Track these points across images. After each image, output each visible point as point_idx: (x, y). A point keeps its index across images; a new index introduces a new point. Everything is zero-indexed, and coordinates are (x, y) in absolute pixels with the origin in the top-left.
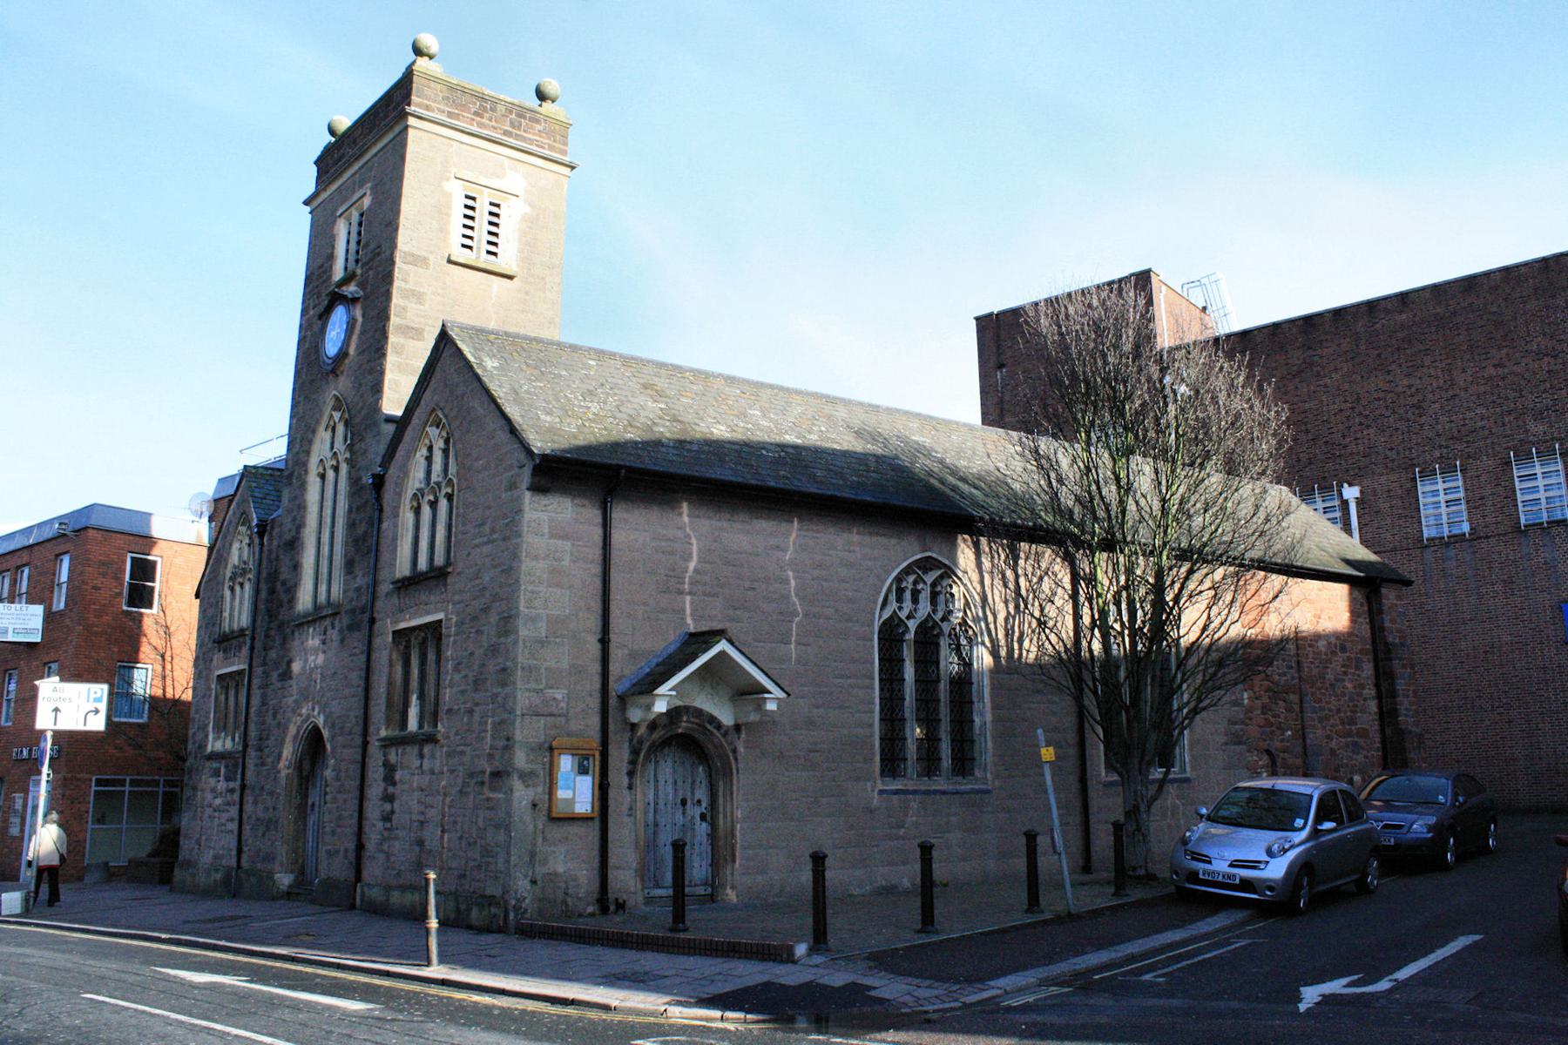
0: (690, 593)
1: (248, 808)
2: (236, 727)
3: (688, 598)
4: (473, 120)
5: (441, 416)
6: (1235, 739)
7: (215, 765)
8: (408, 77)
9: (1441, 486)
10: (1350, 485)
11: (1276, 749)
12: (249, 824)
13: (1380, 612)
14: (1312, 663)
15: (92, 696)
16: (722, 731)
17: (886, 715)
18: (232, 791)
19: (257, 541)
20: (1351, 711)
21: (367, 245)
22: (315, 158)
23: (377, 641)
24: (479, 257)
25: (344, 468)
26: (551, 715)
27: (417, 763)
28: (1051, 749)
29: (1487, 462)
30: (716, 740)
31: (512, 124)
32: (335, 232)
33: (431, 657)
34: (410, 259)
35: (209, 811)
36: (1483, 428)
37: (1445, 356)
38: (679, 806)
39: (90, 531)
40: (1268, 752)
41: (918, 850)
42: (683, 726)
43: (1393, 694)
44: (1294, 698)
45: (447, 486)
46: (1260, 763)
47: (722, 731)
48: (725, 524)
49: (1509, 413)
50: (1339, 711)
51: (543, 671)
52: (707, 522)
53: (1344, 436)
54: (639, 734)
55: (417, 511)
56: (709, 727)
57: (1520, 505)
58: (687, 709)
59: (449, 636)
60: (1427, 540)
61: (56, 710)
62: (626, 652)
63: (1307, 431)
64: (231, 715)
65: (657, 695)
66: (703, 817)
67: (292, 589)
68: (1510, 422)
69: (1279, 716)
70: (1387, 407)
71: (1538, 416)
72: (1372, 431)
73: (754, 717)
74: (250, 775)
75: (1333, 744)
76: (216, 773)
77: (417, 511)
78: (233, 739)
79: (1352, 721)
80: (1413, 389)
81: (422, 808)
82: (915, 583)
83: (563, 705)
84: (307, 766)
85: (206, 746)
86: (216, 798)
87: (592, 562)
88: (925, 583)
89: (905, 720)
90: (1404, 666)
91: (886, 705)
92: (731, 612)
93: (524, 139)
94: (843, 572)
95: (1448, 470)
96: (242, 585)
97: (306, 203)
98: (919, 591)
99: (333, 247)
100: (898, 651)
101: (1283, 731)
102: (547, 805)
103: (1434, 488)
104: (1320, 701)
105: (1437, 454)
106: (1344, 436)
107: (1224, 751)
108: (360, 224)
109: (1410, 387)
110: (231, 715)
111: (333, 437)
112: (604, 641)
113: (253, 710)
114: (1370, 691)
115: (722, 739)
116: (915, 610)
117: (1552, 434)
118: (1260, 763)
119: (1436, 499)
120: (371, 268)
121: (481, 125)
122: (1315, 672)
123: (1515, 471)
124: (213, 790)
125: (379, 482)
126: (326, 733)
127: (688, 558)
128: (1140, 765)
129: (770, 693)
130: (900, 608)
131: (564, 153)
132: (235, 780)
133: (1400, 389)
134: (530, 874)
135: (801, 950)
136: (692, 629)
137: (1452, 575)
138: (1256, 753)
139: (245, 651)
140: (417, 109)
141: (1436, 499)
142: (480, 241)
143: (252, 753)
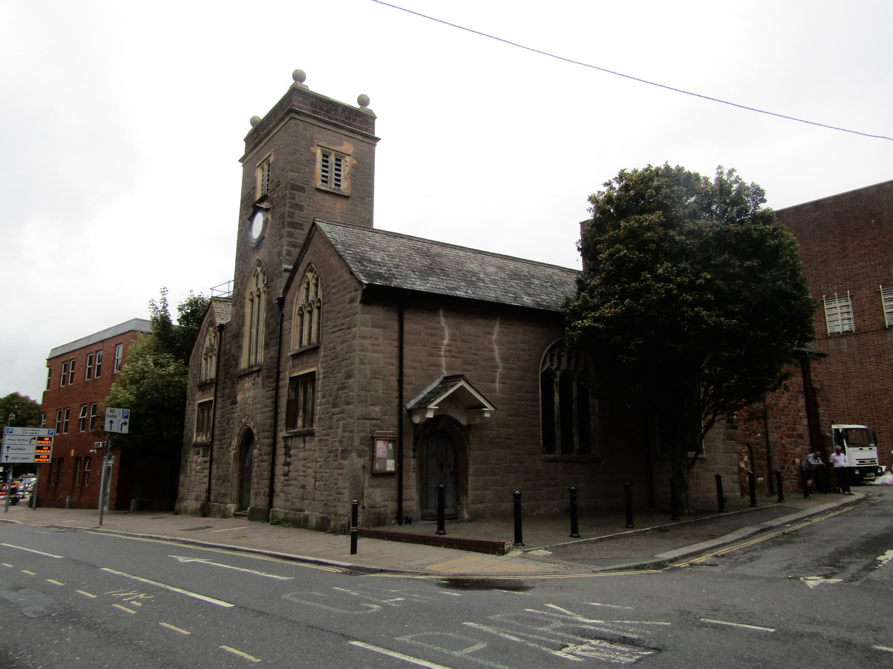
0: (445, 356)
1: (214, 470)
5: (314, 267)
7: (197, 449)
9: (838, 305)
12: (214, 479)
13: (809, 371)
18: (205, 462)
19: (218, 334)
21: (273, 181)
23: (281, 383)
24: (331, 187)
25: (263, 296)
26: (373, 419)
27: (302, 445)
32: (256, 175)
33: (310, 390)
35: (193, 473)
36: (864, 273)
40: (748, 445)
43: (817, 415)
45: (317, 302)
49: (879, 264)
50: (786, 424)
55: (302, 316)
56: (454, 426)
59: (318, 379)
60: (830, 334)
61: (111, 422)
64: (206, 423)
66: (451, 473)
67: (237, 359)
69: (753, 426)
73: (478, 421)
74: (215, 453)
75: (784, 442)
76: (198, 453)
77: (302, 316)
78: (206, 435)
79: (794, 430)
85: (192, 439)
86: (197, 466)
87: (394, 340)
90: (823, 400)
92: (465, 366)
93: (352, 125)
95: (842, 296)
96: (211, 357)
97: (241, 161)
99: (255, 183)
101: (756, 434)
105: (836, 287)
107: (724, 443)
108: (269, 171)
110: (206, 423)
111: (257, 280)
112: (400, 381)
113: (217, 421)
114: (803, 413)
116: (560, 366)
120: (275, 193)
121: (329, 118)
122: (773, 402)
123: (882, 296)
124: (196, 462)
125: (281, 302)
126: (255, 431)
127: (442, 338)
129: (487, 408)
130: (552, 365)
132: (208, 456)
138: (741, 445)
139: (213, 390)
142: (331, 178)
143: (216, 443)
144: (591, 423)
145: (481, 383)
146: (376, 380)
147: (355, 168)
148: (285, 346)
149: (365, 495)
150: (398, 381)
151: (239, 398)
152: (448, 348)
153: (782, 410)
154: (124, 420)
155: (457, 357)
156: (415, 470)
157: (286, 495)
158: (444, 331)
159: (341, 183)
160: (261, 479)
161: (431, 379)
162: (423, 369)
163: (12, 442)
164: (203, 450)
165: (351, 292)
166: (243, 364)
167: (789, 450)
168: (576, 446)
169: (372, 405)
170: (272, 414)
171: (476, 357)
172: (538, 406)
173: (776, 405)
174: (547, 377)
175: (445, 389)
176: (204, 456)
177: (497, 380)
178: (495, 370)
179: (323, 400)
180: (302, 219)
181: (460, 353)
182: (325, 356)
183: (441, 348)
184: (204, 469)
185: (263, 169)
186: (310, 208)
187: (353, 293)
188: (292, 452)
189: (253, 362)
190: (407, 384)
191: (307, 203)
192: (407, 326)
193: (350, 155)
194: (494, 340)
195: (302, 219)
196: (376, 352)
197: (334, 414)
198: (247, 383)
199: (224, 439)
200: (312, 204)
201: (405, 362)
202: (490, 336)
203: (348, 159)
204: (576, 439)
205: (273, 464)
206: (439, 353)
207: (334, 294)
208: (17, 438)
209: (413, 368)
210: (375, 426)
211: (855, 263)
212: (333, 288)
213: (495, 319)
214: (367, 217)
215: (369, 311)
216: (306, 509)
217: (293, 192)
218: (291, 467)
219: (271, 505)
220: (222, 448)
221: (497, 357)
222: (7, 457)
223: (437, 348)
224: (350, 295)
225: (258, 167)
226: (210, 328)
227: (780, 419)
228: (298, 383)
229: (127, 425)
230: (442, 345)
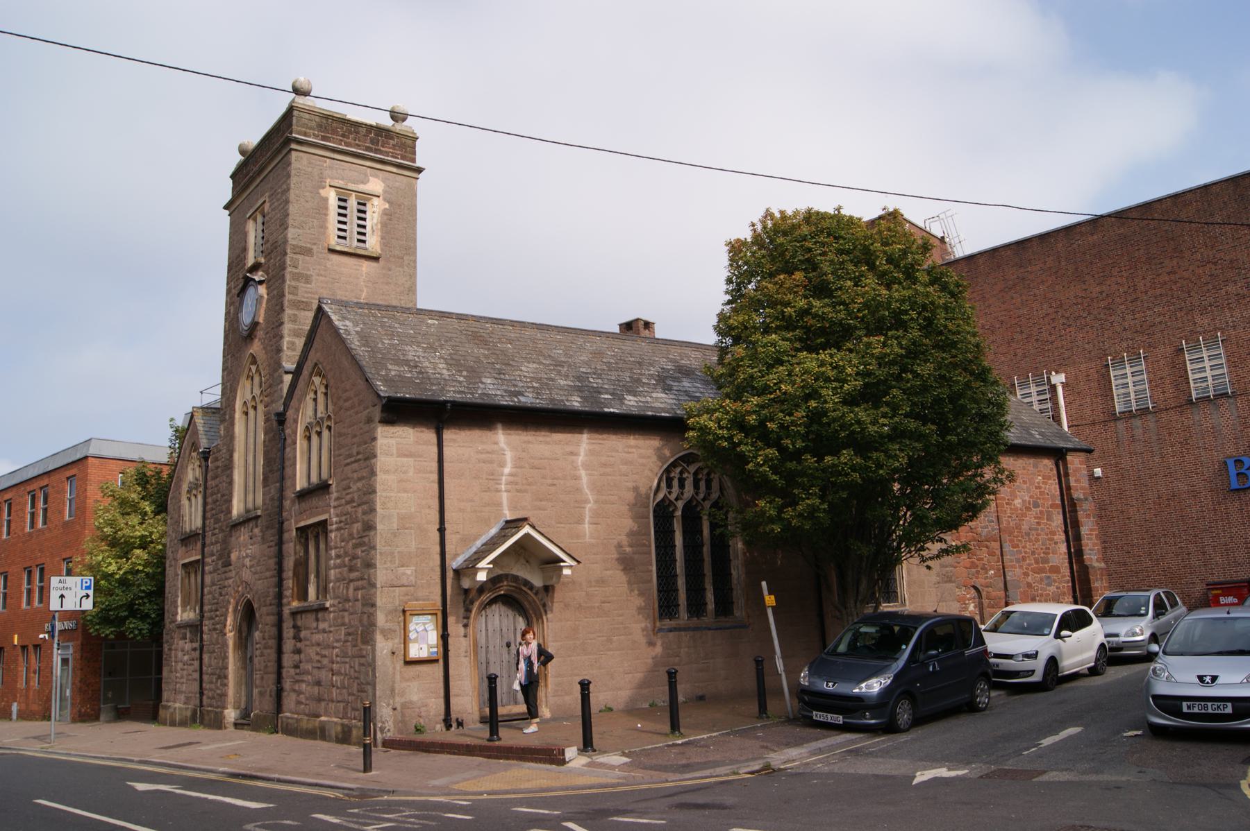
0: (506, 491)
2: (196, 602)
4: (341, 140)
6: (946, 579)
7: (183, 631)
8: (291, 110)
10: (1057, 372)
11: (981, 585)
14: (1009, 517)
15: (84, 585)
17: (662, 573)
18: (194, 649)
20: (1044, 553)
22: (230, 173)
23: (286, 536)
24: (352, 244)
26: (403, 586)
28: (773, 597)
29: (1165, 350)
30: (530, 599)
31: (372, 142)
32: (246, 230)
33: (322, 546)
34: (297, 250)
36: (1160, 323)
37: (1128, 267)
39: (89, 459)
41: (666, 675)
44: (996, 545)
46: (968, 596)
49: (1181, 309)
50: (1033, 553)
51: (396, 554)
52: (517, 437)
53: (1051, 334)
54: (470, 597)
55: (309, 439)
56: (524, 588)
57: (1191, 382)
58: (506, 576)
61: (62, 596)
62: (458, 536)
63: (1022, 332)
65: (479, 568)
68: (1182, 317)
69: (982, 559)
70: (1084, 310)
71: (1204, 311)
72: (1072, 329)
74: (205, 636)
76: (184, 638)
77: (309, 439)
78: (195, 611)
79: (1046, 561)
80: (1104, 295)
81: (318, 658)
82: (681, 473)
83: (412, 578)
84: (245, 628)
88: (689, 473)
89: (677, 576)
91: (662, 565)
92: (538, 503)
93: (381, 152)
94: (624, 468)
96: (195, 496)
97: (226, 208)
98: (685, 479)
100: (670, 525)
101: (986, 571)
102: (403, 652)
103: (1122, 372)
104: (1017, 546)
105: (1125, 344)
106: (1051, 334)
109: (1101, 293)
112: (442, 530)
115: (535, 598)
116: (682, 494)
117: (1215, 325)
118: (968, 596)
119: (1124, 381)
121: (347, 144)
122: (1012, 524)
123: (1186, 356)
124: (183, 651)
125: (281, 419)
127: (502, 465)
128: (856, 603)
129: (564, 561)
130: (670, 493)
131: (414, 160)
133: (1094, 295)
134: (391, 701)
135: (571, 752)
136: (508, 519)
137: (1140, 440)
139: (199, 545)
140: (297, 136)
141: (1124, 381)
142: (352, 232)
143: (206, 622)
144: (733, 571)
147: (386, 214)
148: (288, 483)
149: (396, 691)
150: (445, 529)
151: (234, 556)
152: (511, 479)
153: (1028, 534)
154: (84, 593)
155: (525, 491)
157: (298, 696)
158: (504, 454)
159: (367, 238)
160: (266, 673)
161: (487, 523)
162: (475, 511)
164: (191, 632)
165: (367, 408)
166: (237, 508)
167: (1037, 590)
168: (711, 606)
169: (402, 566)
170: (275, 580)
171: (553, 489)
172: (650, 553)
173: (1018, 527)
174: (663, 513)
175: (506, 537)
176: (191, 641)
177: (587, 520)
178: (583, 505)
179: (338, 561)
180: (310, 295)
181: (529, 485)
182: (337, 499)
183: (501, 480)
184: (193, 660)
185: (255, 220)
187: (371, 409)
188: (303, 634)
189: (250, 505)
190: (452, 534)
191: (315, 271)
193: (379, 197)
194: (580, 464)
195: (310, 295)
196: (405, 491)
197: (352, 581)
198: (243, 535)
199: (217, 616)
200: (323, 273)
202: (573, 457)
203: (376, 201)
204: (710, 596)
205: (280, 652)
206: (497, 486)
207: (347, 410)
209: (460, 510)
211: (1149, 308)
212: (346, 401)
216: (322, 713)
217: (295, 256)
218: (302, 656)
219: (279, 707)
220: (215, 629)
221: (585, 487)
223: (493, 480)
224: (367, 411)
225: (249, 218)
226: (193, 454)
227: (1024, 547)
228: (307, 535)
230: (502, 475)
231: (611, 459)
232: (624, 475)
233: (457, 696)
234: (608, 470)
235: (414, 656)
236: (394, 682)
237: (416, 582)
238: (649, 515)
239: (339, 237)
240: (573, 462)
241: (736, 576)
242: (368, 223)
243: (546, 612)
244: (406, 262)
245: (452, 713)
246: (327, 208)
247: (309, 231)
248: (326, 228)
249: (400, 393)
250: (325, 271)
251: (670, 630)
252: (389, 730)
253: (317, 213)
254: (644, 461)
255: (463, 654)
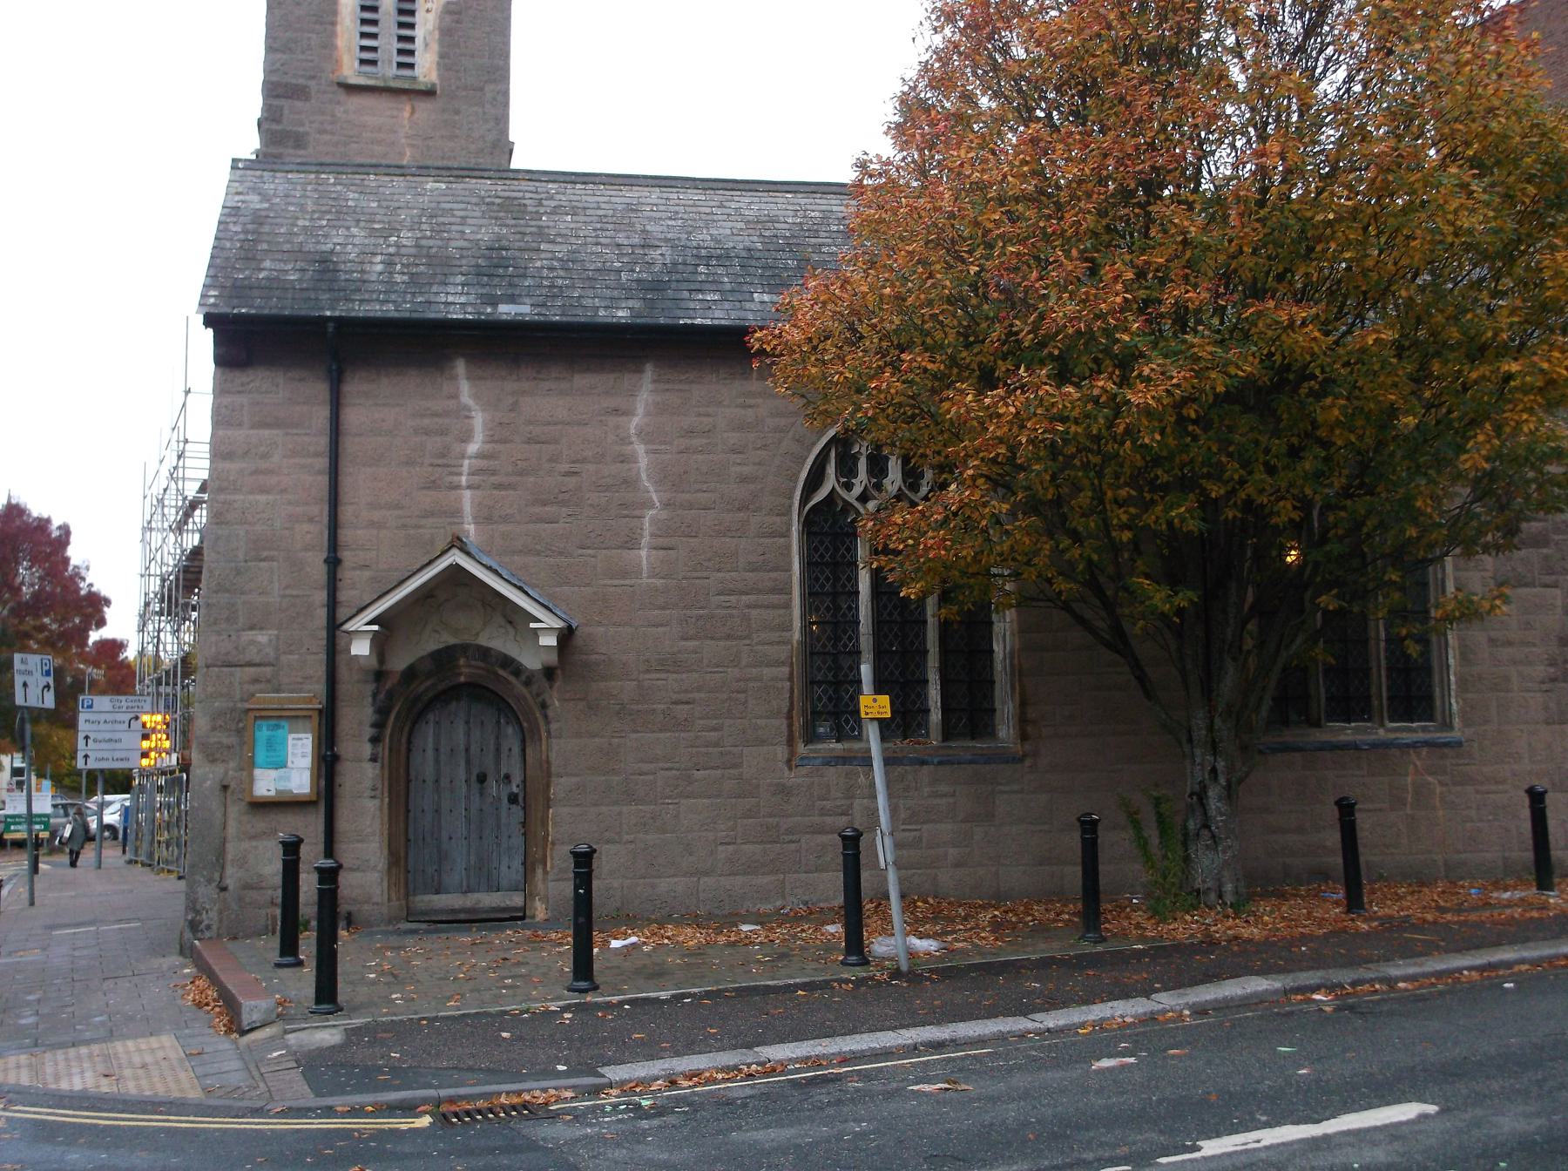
0: (469, 487)
3: (467, 494)
16: (523, 678)
24: (388, 71)
26: (250, 664)
28: (885, 700)
38: (475, 786)
42: (466, 671)
47: (523, 678)
48: (526, 385)
56: (501, 672)
61: (25, 685)
66: (513, 799)
83: (270, 652)
87: (317, 455)
92: (537, 510)
100: (848, 550)
112: (333, 563)
127: (466, 437)
134: (217, 876)
144: (995, 647)
145: (590, 551)
146: (263, 564)
149: (229, 857)
156: (378, 793)
158: (468, 417)
163: (94, 727)
169: (252, 628)
171: (572, 482)
172: (787, 606)
177: (645, 541)
181: (521, 474)
186: (327, 137)
190: (354, 569)
192: (354, 416)
194: (633, 431)
196: (263, 490)
200: (329, 128)
201: (347, 513)
206: (451, 478)
208: (102, 717)
210: (256, 681)
213: (640, 371)
214: (490, 137)
215: (242, 385)
221: (644, 476)
222: (86, 757)
229: (52, 689)
230: (463, 457)
231: (705, 420)
232: (734, 451)
233: (352, 869)
234: (697, 442)
235: (266, 793)
236: (224, 841)
237: (277, 659)
238: (789, 530)
239: (362, 62)
240: (617, 427)
241: (1001, 656)
242: (419, 33)
243: (548, 722)
244: (489, 96)
245: (340, 901)
246: (335, 13)
247: (303, 57)
248: (334, 47)
249: (512, 299)
250: (332, 123)
251: (827, 762)
252: (208, 927)
253: (316, 23)
254: (783, 422)
255: (368, 793)
